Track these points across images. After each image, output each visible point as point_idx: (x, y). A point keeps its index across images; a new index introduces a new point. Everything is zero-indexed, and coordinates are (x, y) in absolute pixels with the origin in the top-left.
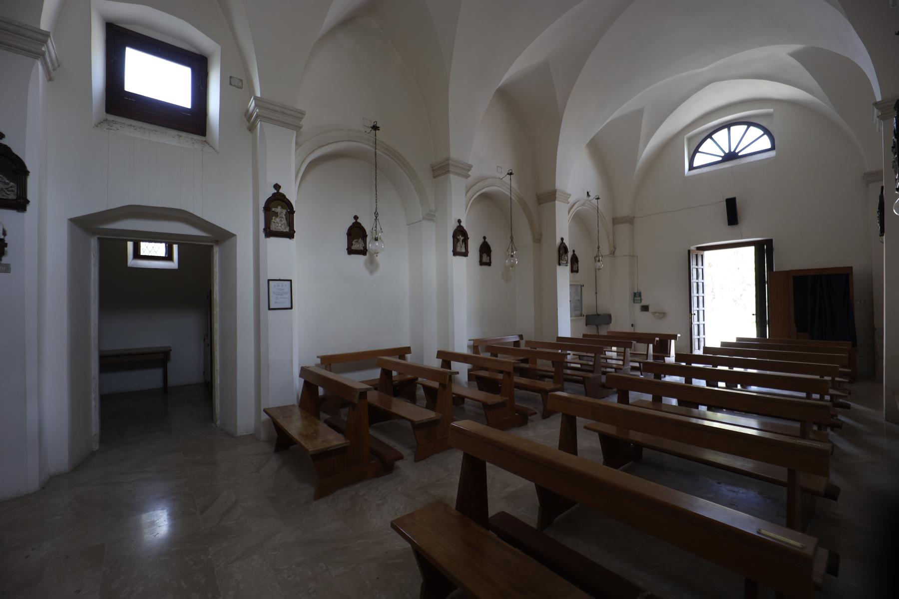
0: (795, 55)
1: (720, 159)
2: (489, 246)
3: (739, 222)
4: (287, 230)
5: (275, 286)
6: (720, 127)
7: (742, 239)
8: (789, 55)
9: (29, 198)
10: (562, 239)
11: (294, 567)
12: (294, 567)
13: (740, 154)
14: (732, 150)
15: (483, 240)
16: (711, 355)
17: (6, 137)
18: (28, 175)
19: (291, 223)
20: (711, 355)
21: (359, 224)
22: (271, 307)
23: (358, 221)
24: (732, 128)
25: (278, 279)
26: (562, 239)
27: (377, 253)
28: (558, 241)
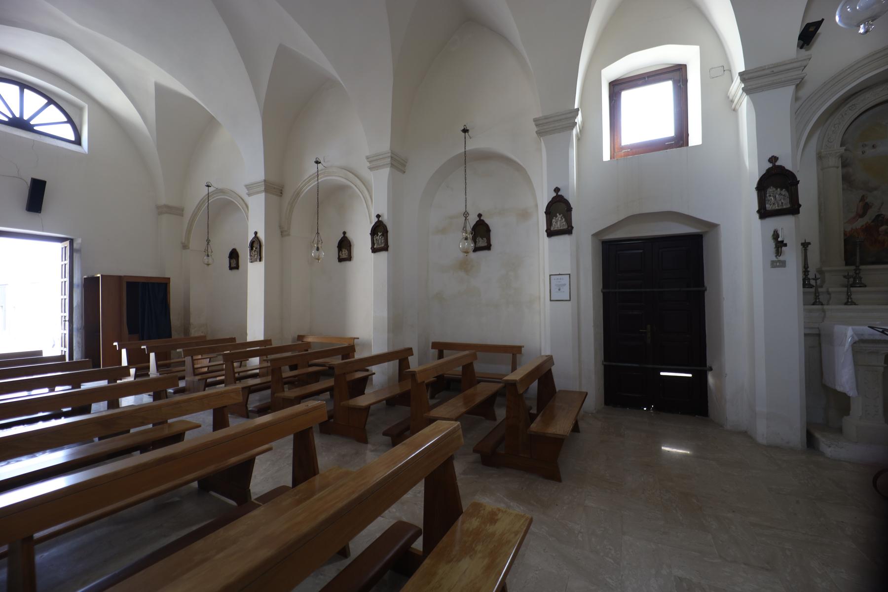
0: (161, 91)
1: (6, 120)
2: (795, 176)
3: (42, 211)
4: (565, 227)
5: (555, 279)
6: (13, 79)
7: (43, 231)
8: (155, 83)
9: (800, 202)
10: (256, 233)
11: (602, 554)
12: (602, 554)
13: (36, 128)
14: (32, 123)
15: (343, 235)
16: (258, 348)
17: (483, 215)
18: (572, 210)
19: (569, 220)
20: (258, 348)
21: (483, 221)
22: (569, 299)
23: (482, 218)
24: (52, 107)
25: (558, 273)
26: (256, 233)
27: (468, 253)
28: (251, 236)
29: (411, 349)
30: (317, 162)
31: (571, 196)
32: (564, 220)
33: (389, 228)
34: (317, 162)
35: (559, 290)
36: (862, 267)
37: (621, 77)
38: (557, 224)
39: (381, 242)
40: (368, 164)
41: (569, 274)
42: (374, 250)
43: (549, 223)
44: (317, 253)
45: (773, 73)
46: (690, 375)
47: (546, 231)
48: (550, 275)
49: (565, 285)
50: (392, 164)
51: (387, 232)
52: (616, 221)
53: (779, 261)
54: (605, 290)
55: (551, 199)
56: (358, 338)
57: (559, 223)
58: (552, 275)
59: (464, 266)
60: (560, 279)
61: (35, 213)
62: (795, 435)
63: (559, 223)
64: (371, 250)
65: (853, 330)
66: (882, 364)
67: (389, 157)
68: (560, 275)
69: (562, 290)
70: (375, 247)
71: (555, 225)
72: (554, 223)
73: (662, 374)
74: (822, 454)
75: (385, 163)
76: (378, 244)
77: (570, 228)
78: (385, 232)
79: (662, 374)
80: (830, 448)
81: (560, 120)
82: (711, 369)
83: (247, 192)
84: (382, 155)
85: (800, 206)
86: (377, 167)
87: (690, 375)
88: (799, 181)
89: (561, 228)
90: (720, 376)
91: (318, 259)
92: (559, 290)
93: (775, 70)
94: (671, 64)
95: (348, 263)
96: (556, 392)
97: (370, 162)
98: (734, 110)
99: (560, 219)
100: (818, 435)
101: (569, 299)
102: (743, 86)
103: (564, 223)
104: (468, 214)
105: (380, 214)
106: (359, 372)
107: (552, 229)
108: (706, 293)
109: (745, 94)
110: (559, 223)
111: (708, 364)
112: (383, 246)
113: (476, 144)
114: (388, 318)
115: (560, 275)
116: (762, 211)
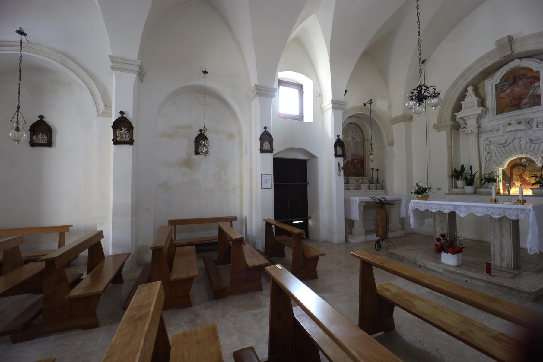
22: (271, 188)
25: (265, 174)
29: (441, 188)
30: (21, 33)
31: (272, 132)
32: (269, 145)
33: (134, 125)
34: (21, 33)
35: (266, 182)
36: (349, 177)
37: (280, 78)
38: (266, 146)
39: (126, 136)
40: (111, 63)
41: (271, 175)
42: (262, 151)
43: (262, 145)
44: (17, 134)
45: (339, 104)
46: (302, 222)
47: (113, 140)
48: (262, 175)
49: (269, 180)
50: (139, 73)
51: (132, 128)
52: (283, 149)
53: (339, 174)
54: (306, 183)
55: (117, 118)
56: (72, 226)
57: (267, 146)
58: (263, 174)
59: (187, 163)
60: (267, 177)
61: (452, 110)
62: (343, 239)
63: (267, 146)
64: (260, 151)
65: (359, 199)
66: (362, 209)
67: (137, 65)
68: (266, 174)
69: (267, 183)
70: (118, 139)
71: (265, 147)
72: (265, 146)
73: (293, 222)
74: (350, 243)
75: (133, 69)
76: (122, 137)
77: (132, 141)
78: (130, 128)
79: (293, 222)
80: (352, 240)
81: (133, 64)
82: (310, 218)
83: (111, 64)
84: (116, 58)
85: (113, 140)
86: (122, 69)
87: (302, 222)
88: (20, 28)
89: (268, 149)
90: (317, 219)
91: (18, 141)
92: (266, 182)
93: (340, 103)
94: (296, 81)
95: (46, 149)
96: (104, 257)
97: (113, 62)
98: (323, 112)
99: (267, 144)
100: (348, 236)
101: (271, 188)
102: (256, 91)
103: (269, 147)
104: (206, 129)
105: (124, 111)
106: (30, 263)
107: (263, 149)
108: (308, 186)
109: (137, 73)
110: (266, 146)
111: (309, 216)
112: (128, 140)
113: (211, 83)
114: (132, 203)
115: (266, 174)
116: (115, 141)
